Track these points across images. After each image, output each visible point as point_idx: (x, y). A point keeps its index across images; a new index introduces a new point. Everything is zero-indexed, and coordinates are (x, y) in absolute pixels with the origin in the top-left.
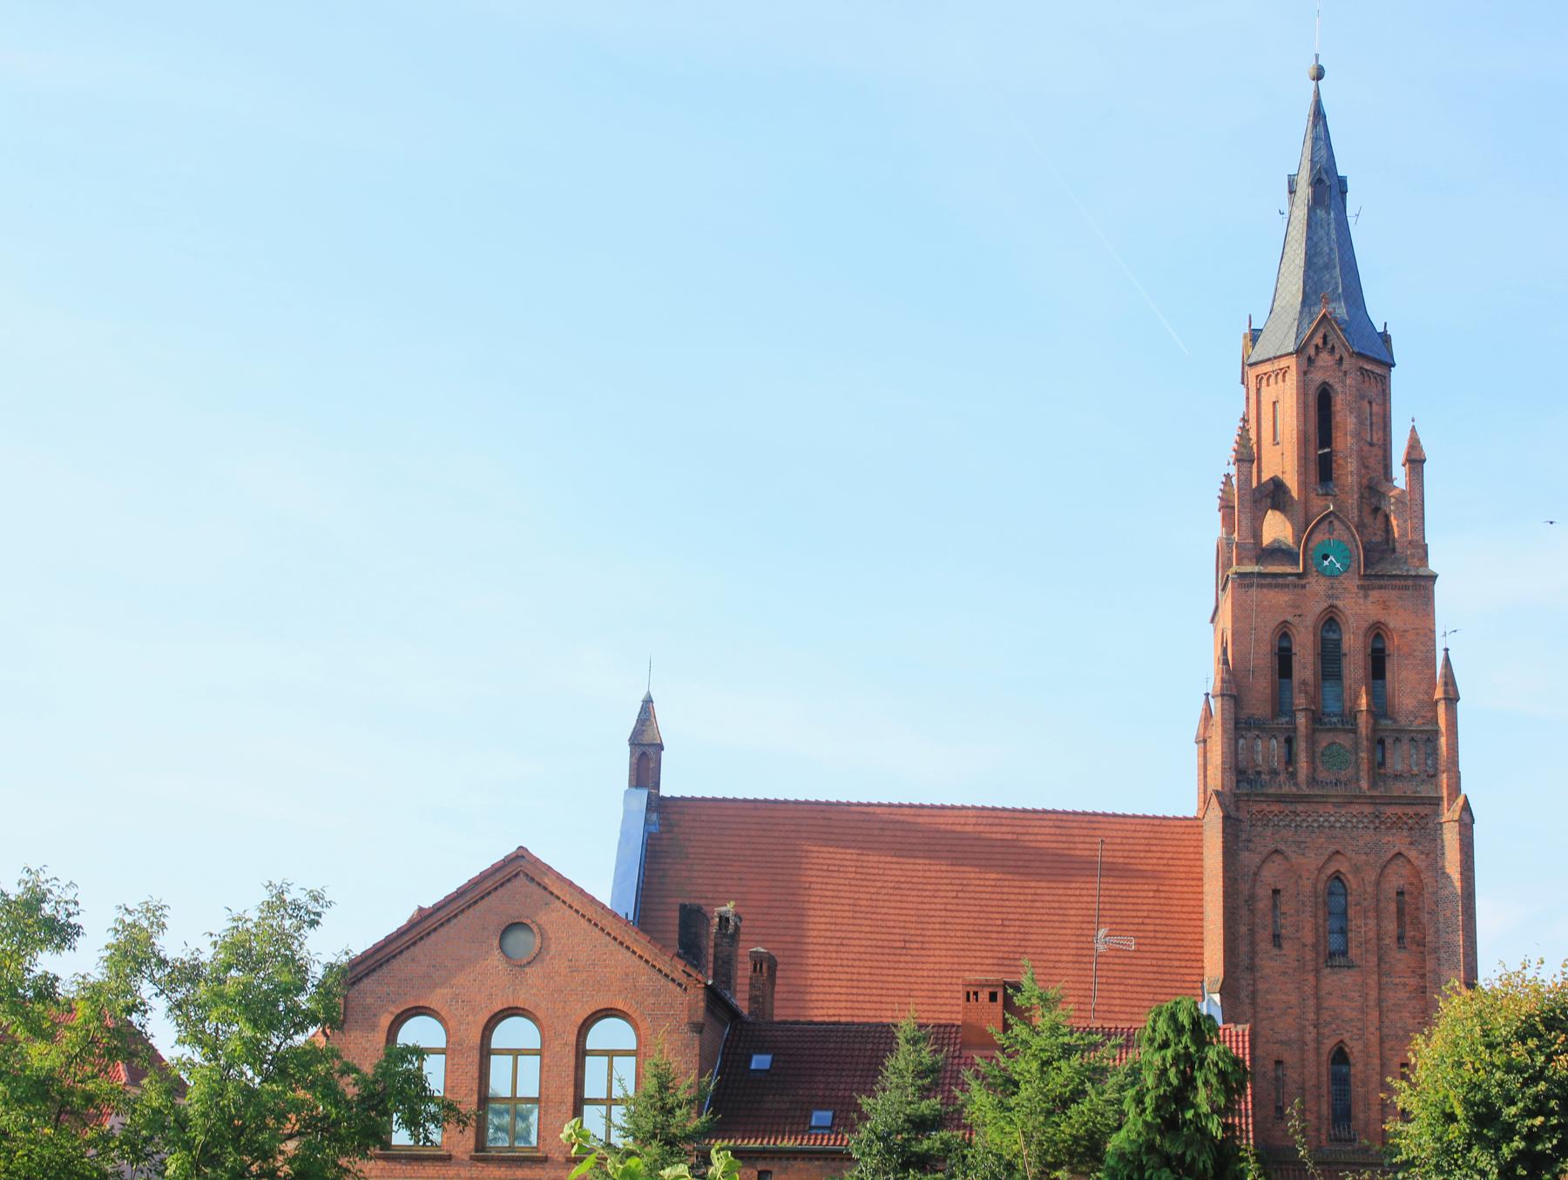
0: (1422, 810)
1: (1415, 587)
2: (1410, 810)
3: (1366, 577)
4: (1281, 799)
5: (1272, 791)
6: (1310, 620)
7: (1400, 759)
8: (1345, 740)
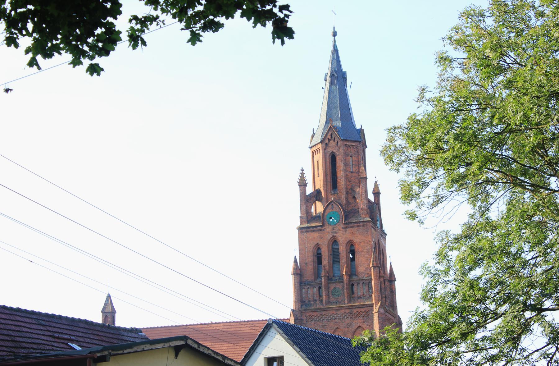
0: (367, 309)
1: (363, 226)
2: (363, 310)
3: (345, 224)
4: (316, 310)
5: (313, 308)
6: (326, 243)
7: (359, 291)
8: (339, 286)
